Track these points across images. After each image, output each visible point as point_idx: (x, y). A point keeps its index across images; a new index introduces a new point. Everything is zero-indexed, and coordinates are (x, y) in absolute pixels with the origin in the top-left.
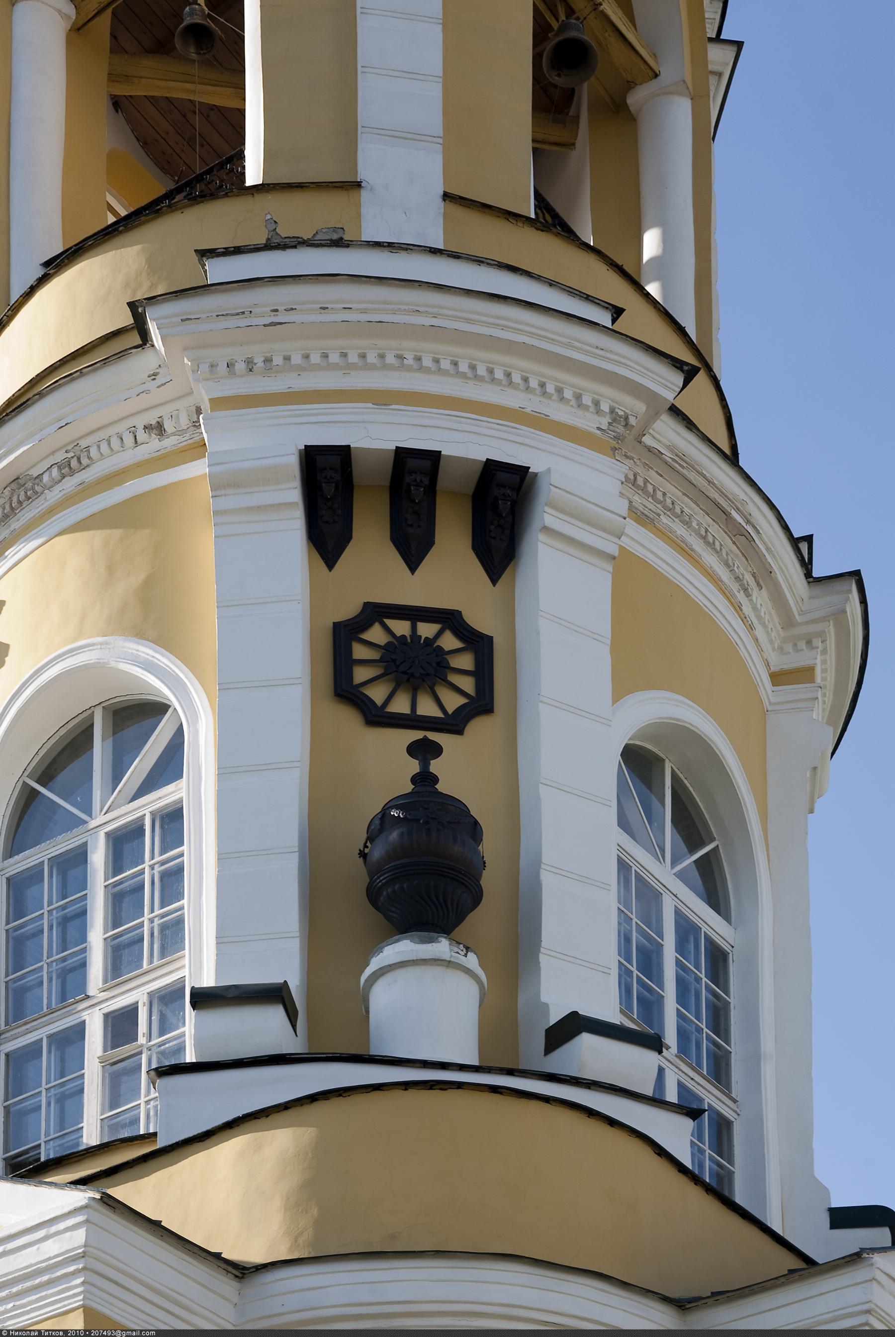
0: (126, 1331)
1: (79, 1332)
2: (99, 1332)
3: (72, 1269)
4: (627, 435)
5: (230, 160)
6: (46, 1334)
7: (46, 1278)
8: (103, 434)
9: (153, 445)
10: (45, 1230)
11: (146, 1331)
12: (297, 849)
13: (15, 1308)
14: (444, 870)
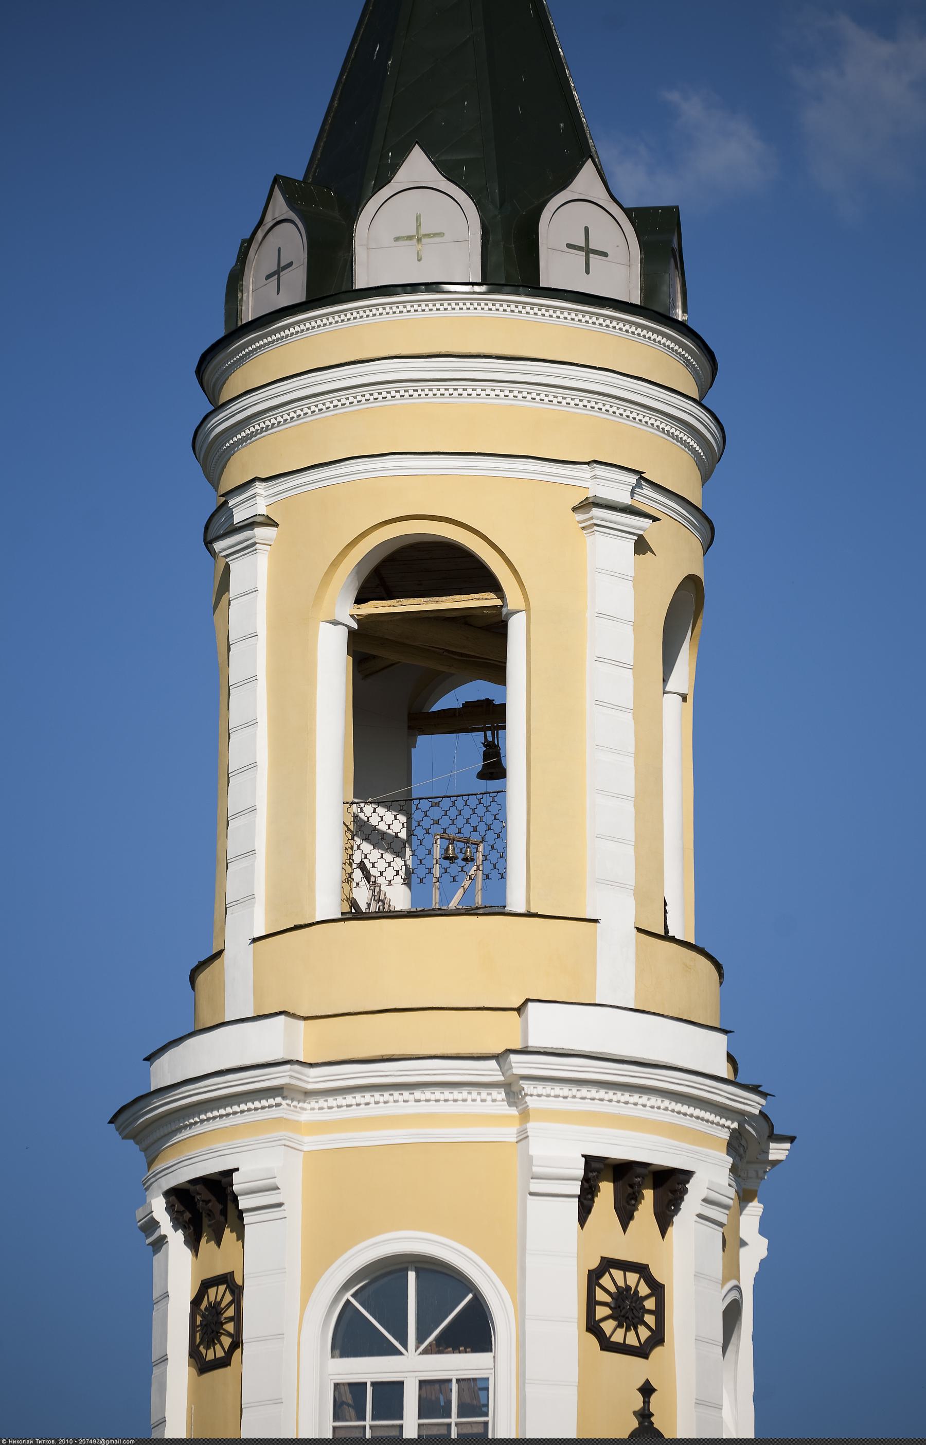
0: (109, 1440)
1: (69, 1441)
5: (632, 1437)
12: (770, 1151)
14: (678, 359)
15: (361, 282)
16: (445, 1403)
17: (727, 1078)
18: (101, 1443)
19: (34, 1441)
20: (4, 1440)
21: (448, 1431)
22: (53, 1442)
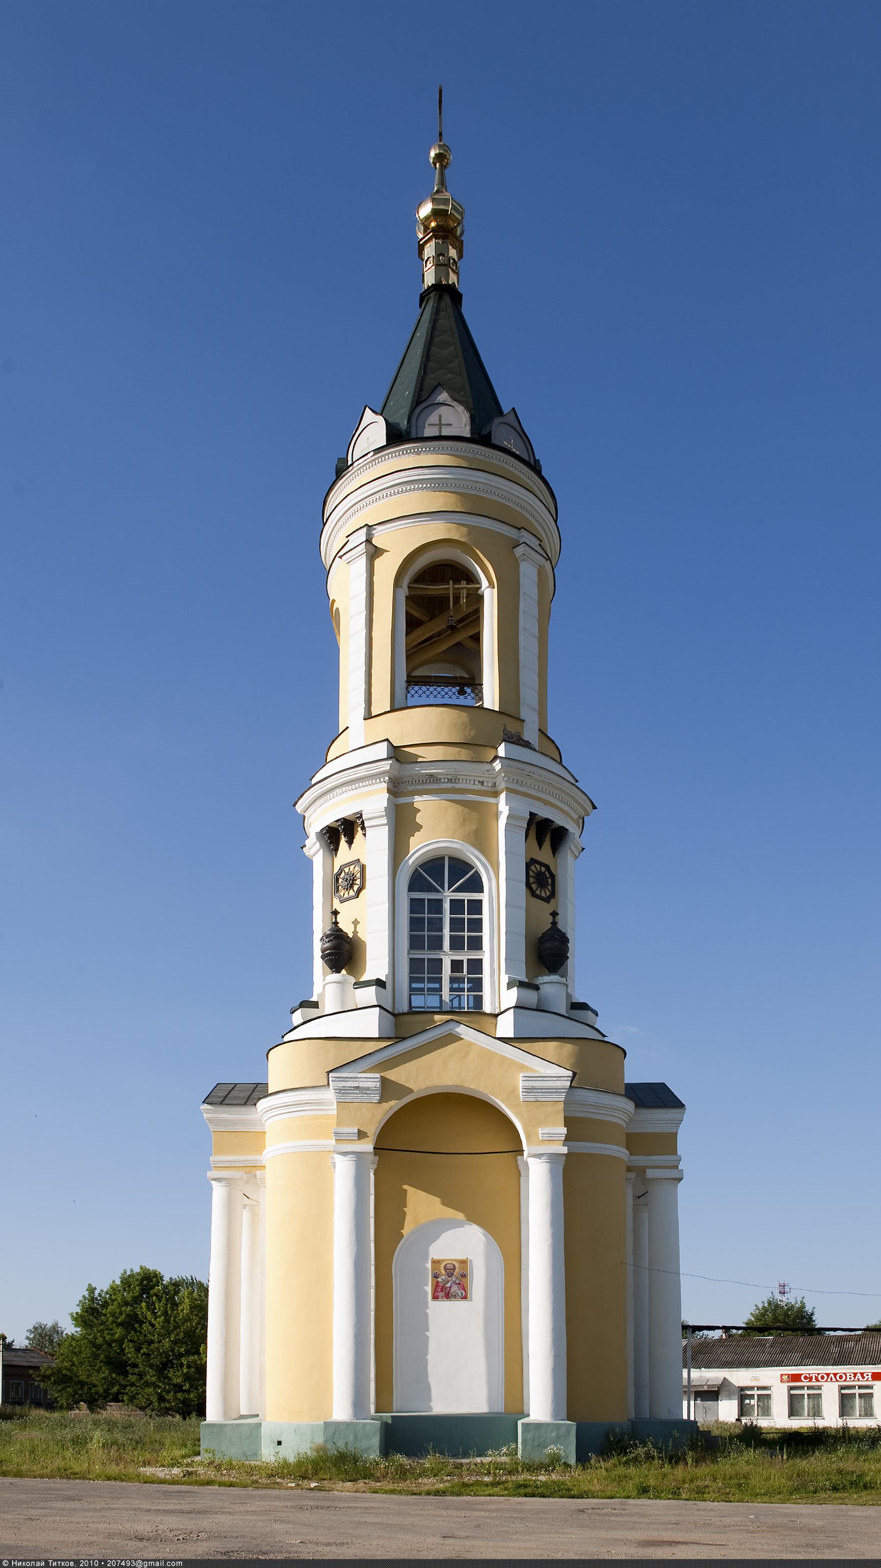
0: (148, 1561)
2: (117, 1563)
4: (732, 1457)
6: (55, 1564)
8: (470, 778)
9: (478, 787)
11: (171, 1560)
16: (449, 582)
18: (137, 1565)
19: (46, 1561)
20: (5, 1561)
21: (432, 239)
22: (72, 1564)
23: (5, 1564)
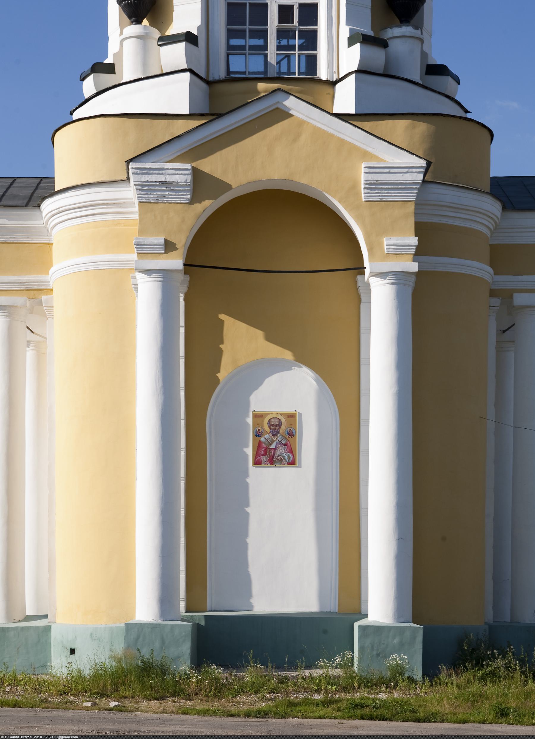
0: (63, 736)
3: (415, 187)
7: (403, 187)
10: (407, 169)
11: (73, 736)
13: (388, 193)
15: (57, 188)
17: (205, 78)
22: (31, 737)
23: (2, 737)
